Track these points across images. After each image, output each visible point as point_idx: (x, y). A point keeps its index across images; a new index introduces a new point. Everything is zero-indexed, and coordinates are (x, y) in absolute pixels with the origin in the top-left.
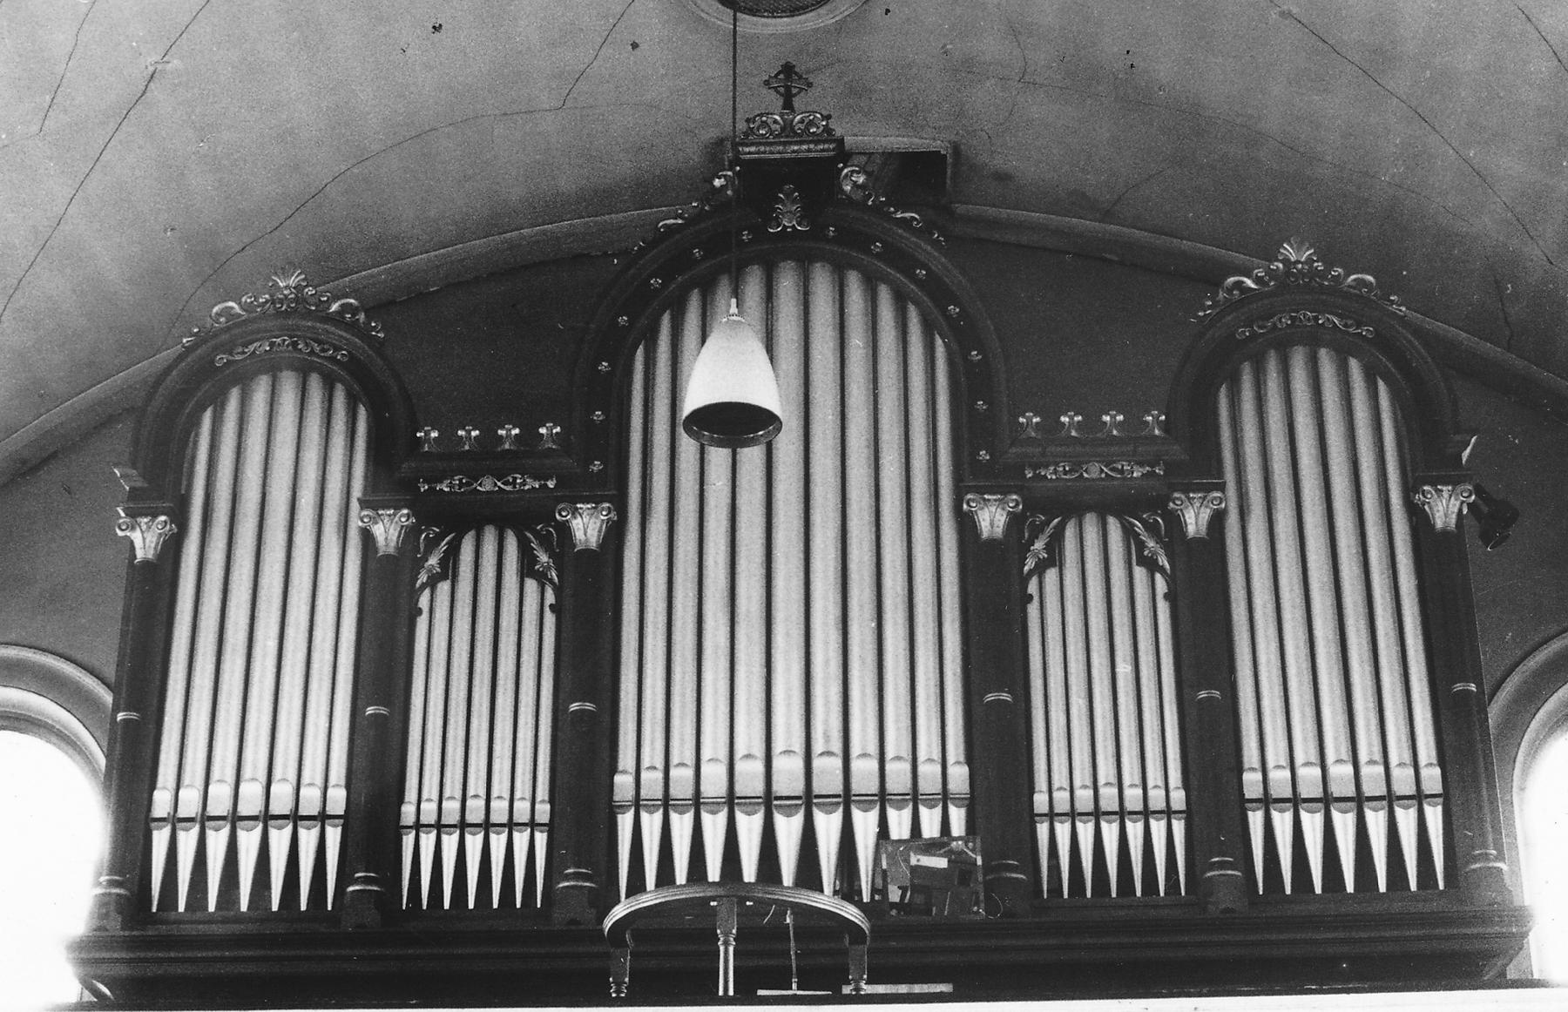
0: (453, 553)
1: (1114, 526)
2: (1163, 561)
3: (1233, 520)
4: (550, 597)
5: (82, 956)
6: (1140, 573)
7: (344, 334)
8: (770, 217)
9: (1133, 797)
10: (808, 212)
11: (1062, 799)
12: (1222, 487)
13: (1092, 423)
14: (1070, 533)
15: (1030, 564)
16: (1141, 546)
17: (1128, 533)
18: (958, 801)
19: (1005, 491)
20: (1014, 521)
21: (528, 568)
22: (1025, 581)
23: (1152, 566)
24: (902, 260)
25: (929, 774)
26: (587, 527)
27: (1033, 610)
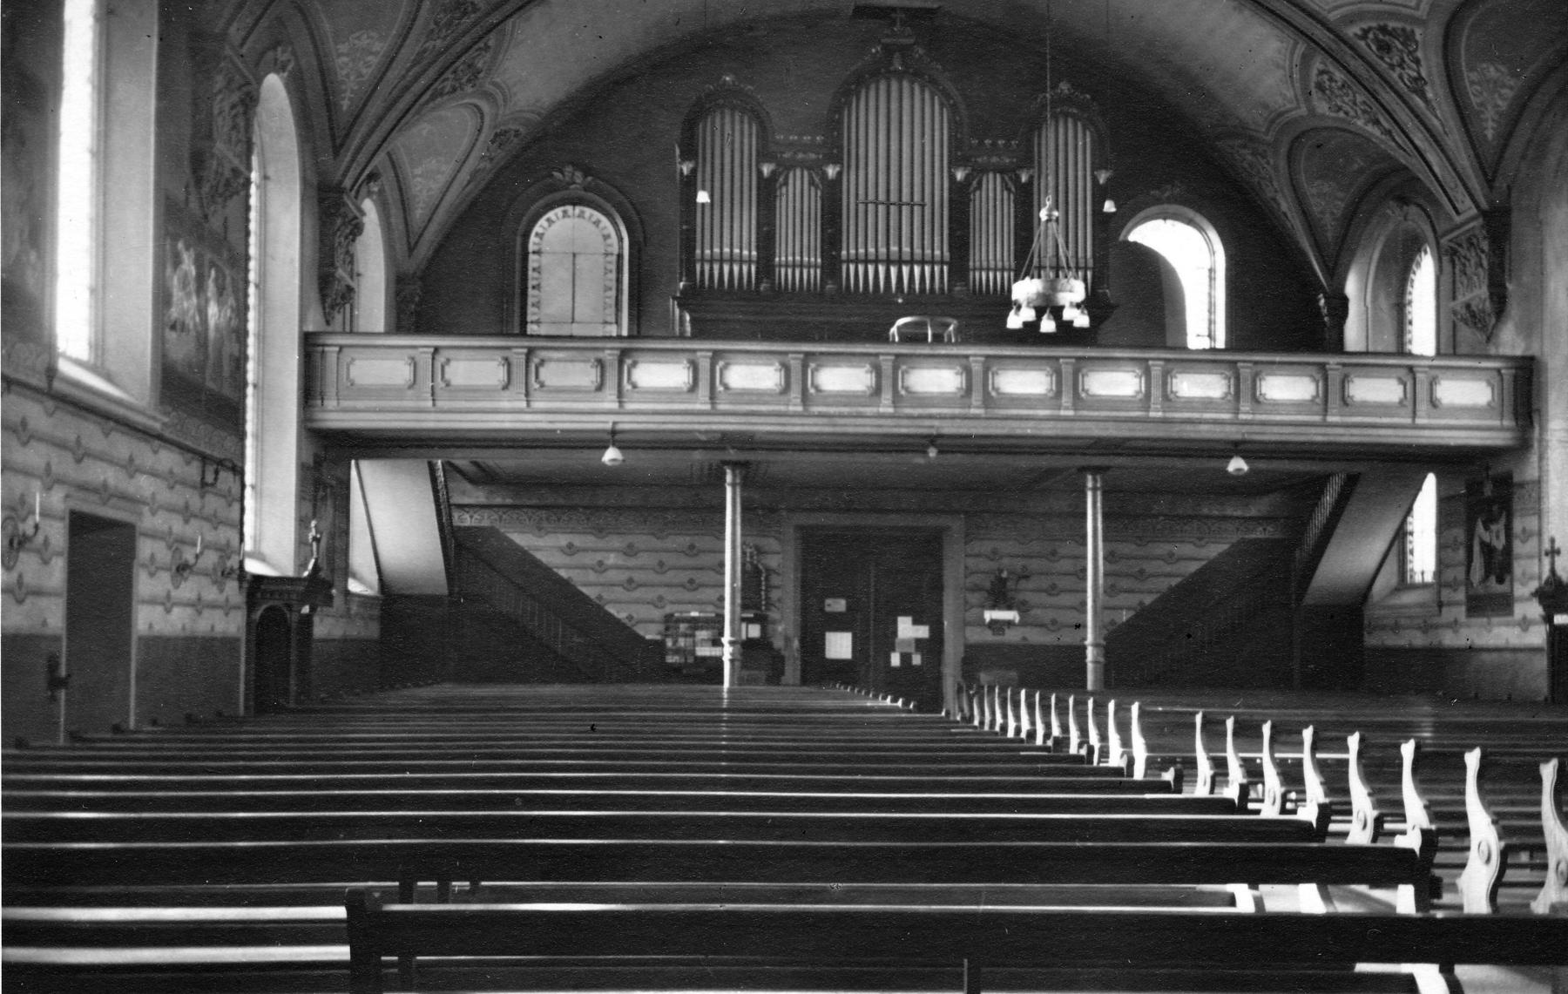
0: (787, 178)
1: (806, 173)
2: (1013, 189)
3: (700, 169)
4: (819, 193)
5: (866, 369)
6: (813, 189)
7: (1463, 45)
8: (891, 64)
9: (992, 264)
10: (904, 63)
11: (978, 264)
12: (1033, 167)
13: (994, 144)
14: (791, 175)
15: (972, 189)
16: (1007, 185)
17: (1003, 179)
18: (947, 263)
19: (966, 166)
20: (967, 177)
21: (812, 183)
22: (969, 194)
23: (1009, 190)
24: (933, 81)
25: (1006, 264)
26: (831, 171)
27: (971, 204)
